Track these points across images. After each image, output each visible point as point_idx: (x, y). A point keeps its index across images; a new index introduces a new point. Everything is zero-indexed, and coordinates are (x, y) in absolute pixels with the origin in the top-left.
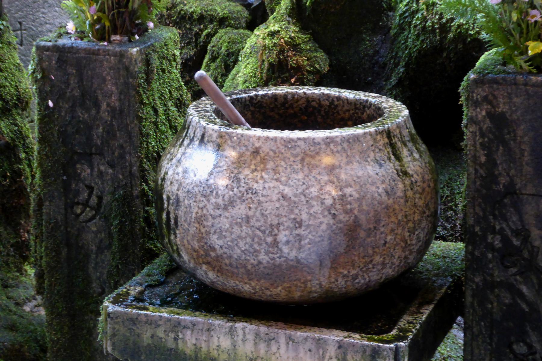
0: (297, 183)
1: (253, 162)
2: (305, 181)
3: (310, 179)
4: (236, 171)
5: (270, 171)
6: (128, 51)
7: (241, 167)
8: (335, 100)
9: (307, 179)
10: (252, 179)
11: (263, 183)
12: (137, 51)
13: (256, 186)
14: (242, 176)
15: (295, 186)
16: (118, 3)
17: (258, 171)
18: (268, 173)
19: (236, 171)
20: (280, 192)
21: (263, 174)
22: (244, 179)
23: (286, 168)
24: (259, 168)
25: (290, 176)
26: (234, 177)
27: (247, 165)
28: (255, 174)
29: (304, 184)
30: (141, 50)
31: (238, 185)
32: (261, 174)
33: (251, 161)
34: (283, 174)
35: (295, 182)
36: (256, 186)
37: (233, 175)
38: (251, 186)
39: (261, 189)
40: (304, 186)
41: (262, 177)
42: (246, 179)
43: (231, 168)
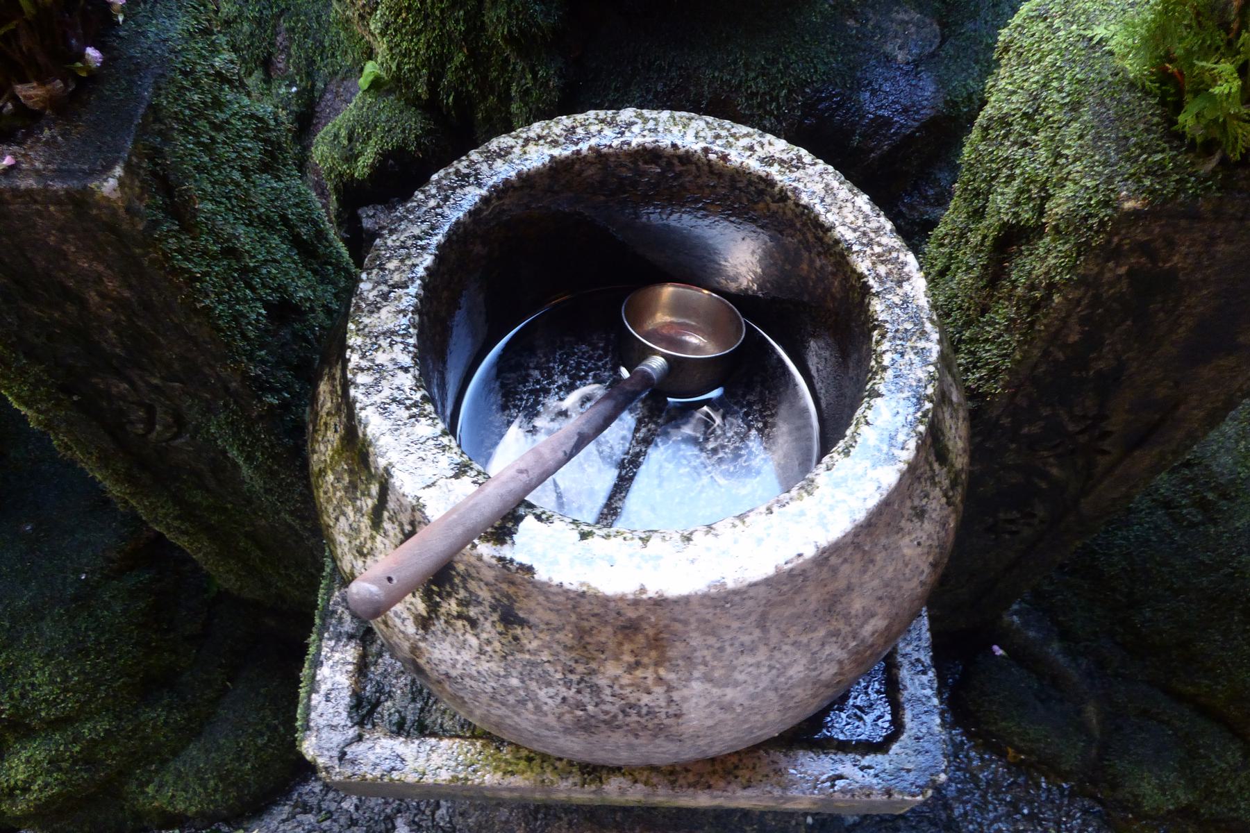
0: (755, 672)
1: (627, 647)
2: (773, 663)
3: (785, 653)
4: (581, 668)
5: (680, 662)
6: (93, 192)
7: (594, 659)
8: (676, 161)
9: (777, 654)
10: (631, 685)
11: (667, 691)
12: (121, 183)
13: (646, 699)
14: (602, 681)
15: (749, 681)
16: (3, 376)
17: (646, 667)
18: (674, 668)
19: (581, 668)
20: (713, 703)
21: (662, 672)
22: (611, 687)
23: (721, 649)
24: (645, 660)
25: (735, 662)
26: (579, 683)
27: (607, 653)
28: (639, 673)
29: (771, 668)
30: (129, 168)
31: (596, 700)
32: (656, 672)
33: (620, 644)
34: (715, 663)
35: (749, 673)
36: (646, 699)
37: (575, 678)
38: (633, 700)
39: (663, 704)
40: (774, 672)
41: (660, 679)
42: (616, 687)
43: (562, 658)
